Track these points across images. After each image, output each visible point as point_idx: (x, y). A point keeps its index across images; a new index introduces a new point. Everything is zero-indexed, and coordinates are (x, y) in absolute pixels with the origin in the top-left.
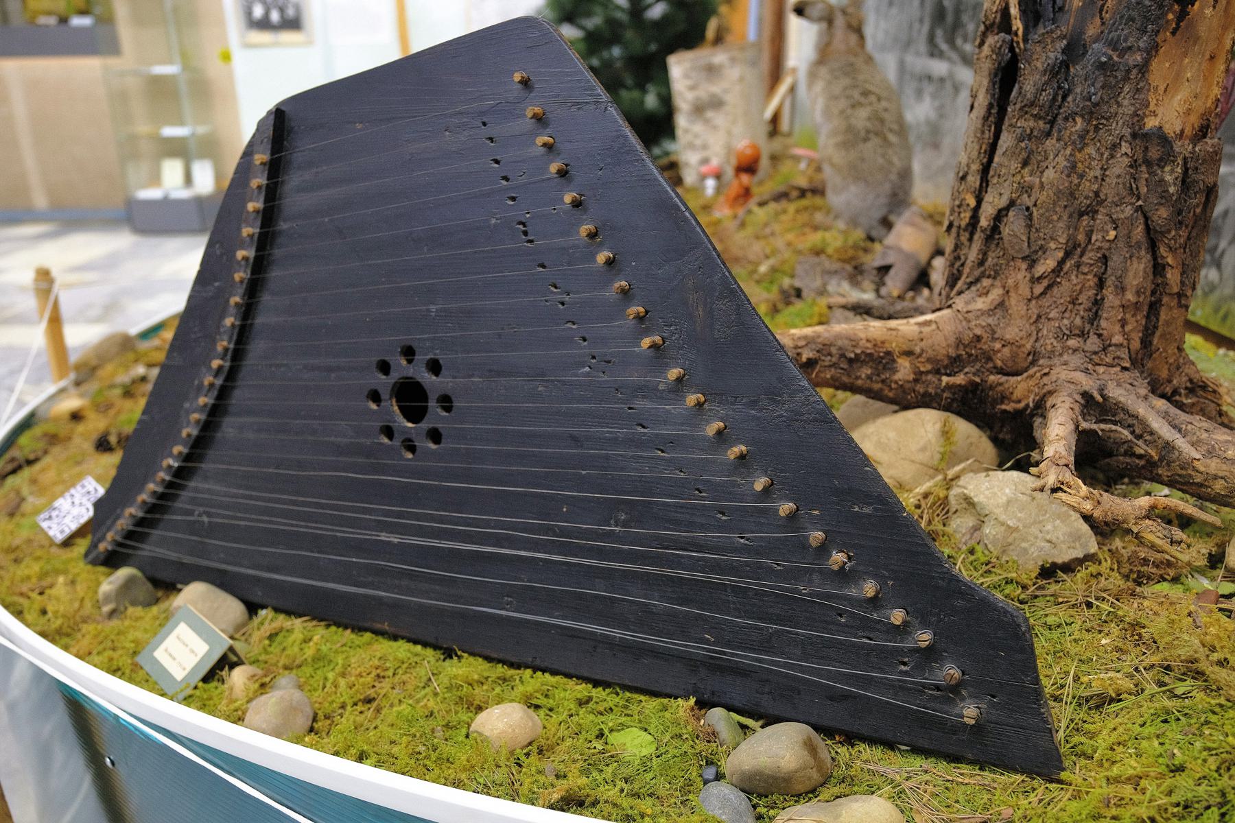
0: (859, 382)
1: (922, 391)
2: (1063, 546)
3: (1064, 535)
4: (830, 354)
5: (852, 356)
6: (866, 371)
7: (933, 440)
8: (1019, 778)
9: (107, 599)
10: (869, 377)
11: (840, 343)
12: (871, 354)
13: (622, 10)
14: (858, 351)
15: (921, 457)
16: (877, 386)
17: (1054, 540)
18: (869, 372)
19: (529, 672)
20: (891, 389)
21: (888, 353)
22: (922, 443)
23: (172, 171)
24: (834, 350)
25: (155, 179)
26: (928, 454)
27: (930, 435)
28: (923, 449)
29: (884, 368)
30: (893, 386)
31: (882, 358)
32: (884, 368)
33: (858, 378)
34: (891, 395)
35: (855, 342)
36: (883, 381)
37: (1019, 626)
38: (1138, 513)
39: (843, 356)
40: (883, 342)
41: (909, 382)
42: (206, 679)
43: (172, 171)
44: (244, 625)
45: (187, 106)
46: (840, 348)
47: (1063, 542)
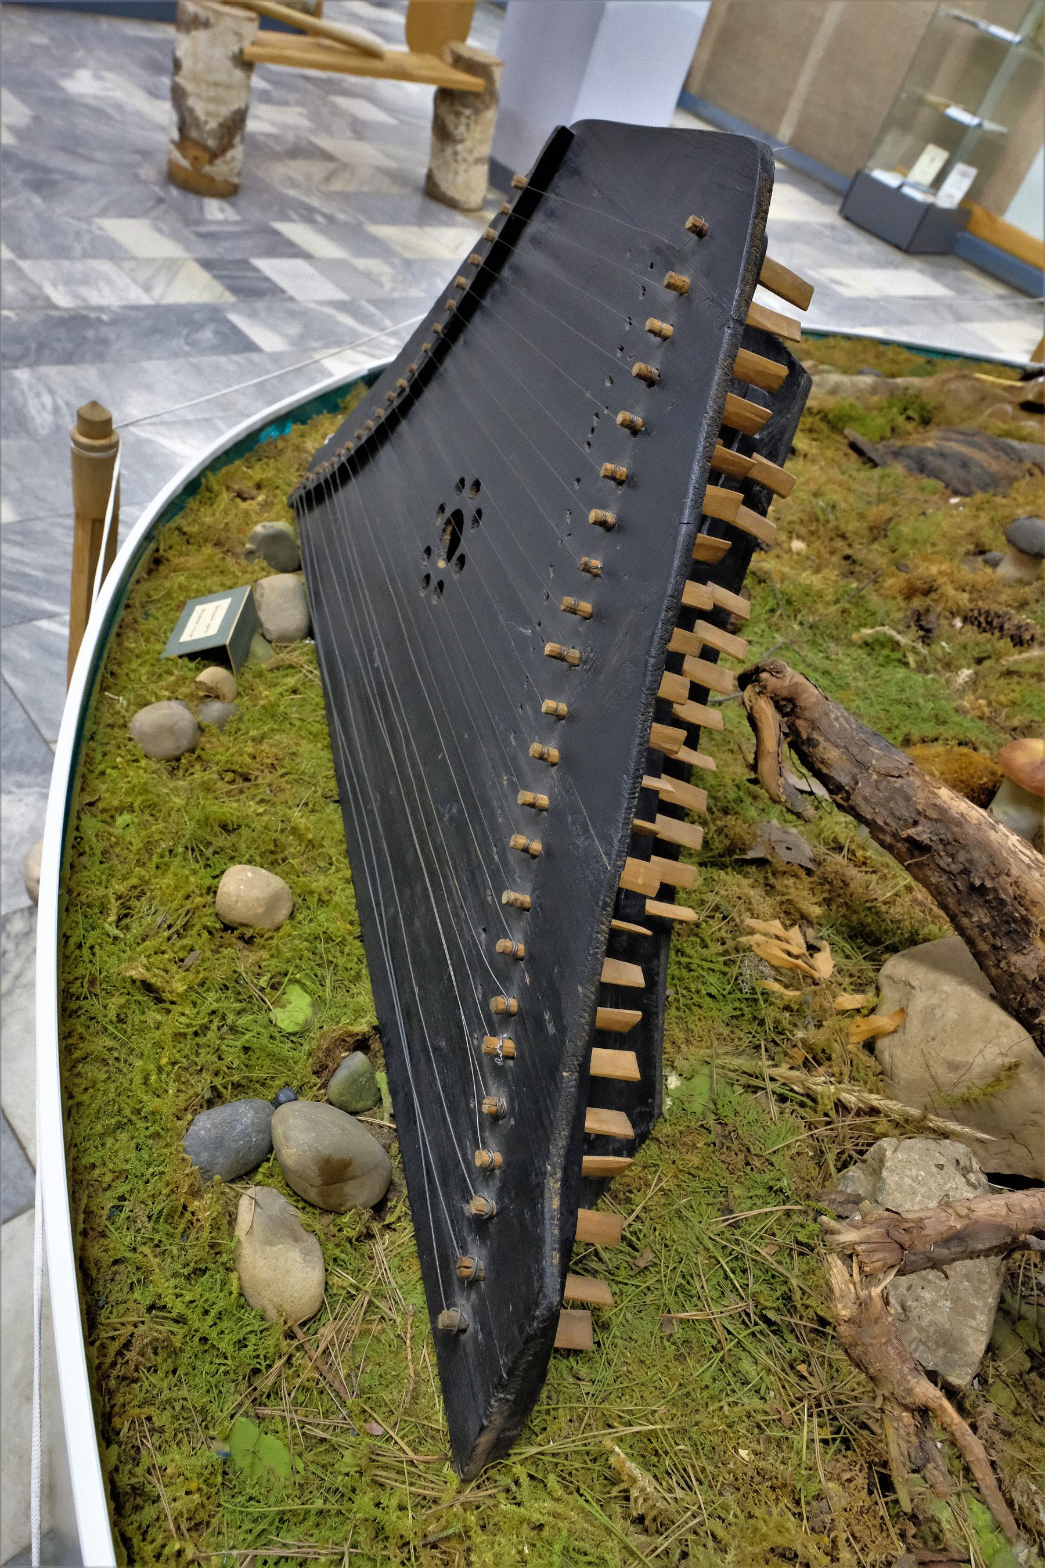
0: (965, 921)
1: (1032, 1004)
2: (915, 1333)
3: (932, 1323)
4: (952, 856)
5: (978, 883)
6: (981, 915)
7: (977, 1070)
8: (440, 1421)
9: (253, 539)
10: (982, 928)
11: (976, 854)
12: (1002, 902)
13: (162, 129)
14: (989, 884)
15: (940, 1071)
16: (983, 947)
17: (914, 1314)
18: (986, 920)
19: (348, 873)
20: (997, 966)
21: (1026, 921)
22: (959, 1058)
23: (930, 161)
24: (962, 856)
25: (906, 163)
26: (952, 1077)
27: (979, 1060)
28: (953, 1066)
29: (1008, 933)
30: (1003, 964)
31: (1015, 921)
32: (1008, 933)
33: (966, 914)
34: (994, 972)
35: (999, 870)
36: (994, 947)
37: (537, 1305)
38: (899, 1392)
39: (966, 872)
40: (1034, 903)
41: (1025, 979)
42: (192, 656)
43: (930, 161)
44: (290, 639)
45: (998, 86)
46: (971, 861)
47: (920, 1329)
